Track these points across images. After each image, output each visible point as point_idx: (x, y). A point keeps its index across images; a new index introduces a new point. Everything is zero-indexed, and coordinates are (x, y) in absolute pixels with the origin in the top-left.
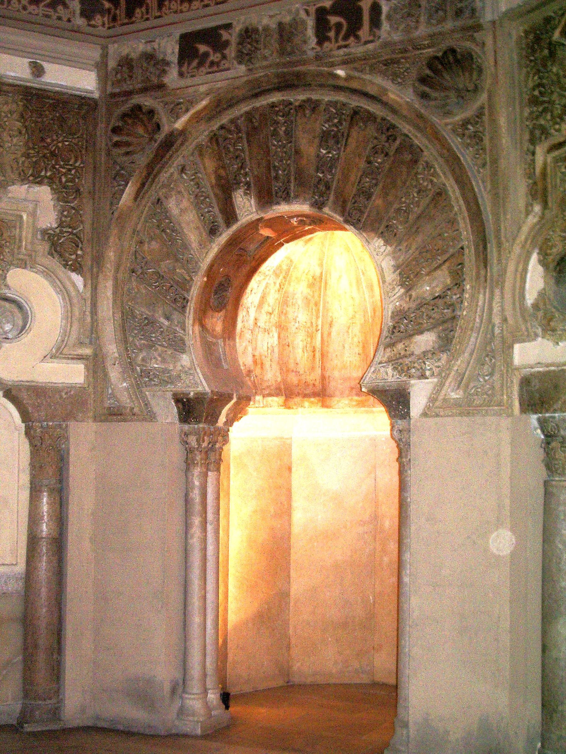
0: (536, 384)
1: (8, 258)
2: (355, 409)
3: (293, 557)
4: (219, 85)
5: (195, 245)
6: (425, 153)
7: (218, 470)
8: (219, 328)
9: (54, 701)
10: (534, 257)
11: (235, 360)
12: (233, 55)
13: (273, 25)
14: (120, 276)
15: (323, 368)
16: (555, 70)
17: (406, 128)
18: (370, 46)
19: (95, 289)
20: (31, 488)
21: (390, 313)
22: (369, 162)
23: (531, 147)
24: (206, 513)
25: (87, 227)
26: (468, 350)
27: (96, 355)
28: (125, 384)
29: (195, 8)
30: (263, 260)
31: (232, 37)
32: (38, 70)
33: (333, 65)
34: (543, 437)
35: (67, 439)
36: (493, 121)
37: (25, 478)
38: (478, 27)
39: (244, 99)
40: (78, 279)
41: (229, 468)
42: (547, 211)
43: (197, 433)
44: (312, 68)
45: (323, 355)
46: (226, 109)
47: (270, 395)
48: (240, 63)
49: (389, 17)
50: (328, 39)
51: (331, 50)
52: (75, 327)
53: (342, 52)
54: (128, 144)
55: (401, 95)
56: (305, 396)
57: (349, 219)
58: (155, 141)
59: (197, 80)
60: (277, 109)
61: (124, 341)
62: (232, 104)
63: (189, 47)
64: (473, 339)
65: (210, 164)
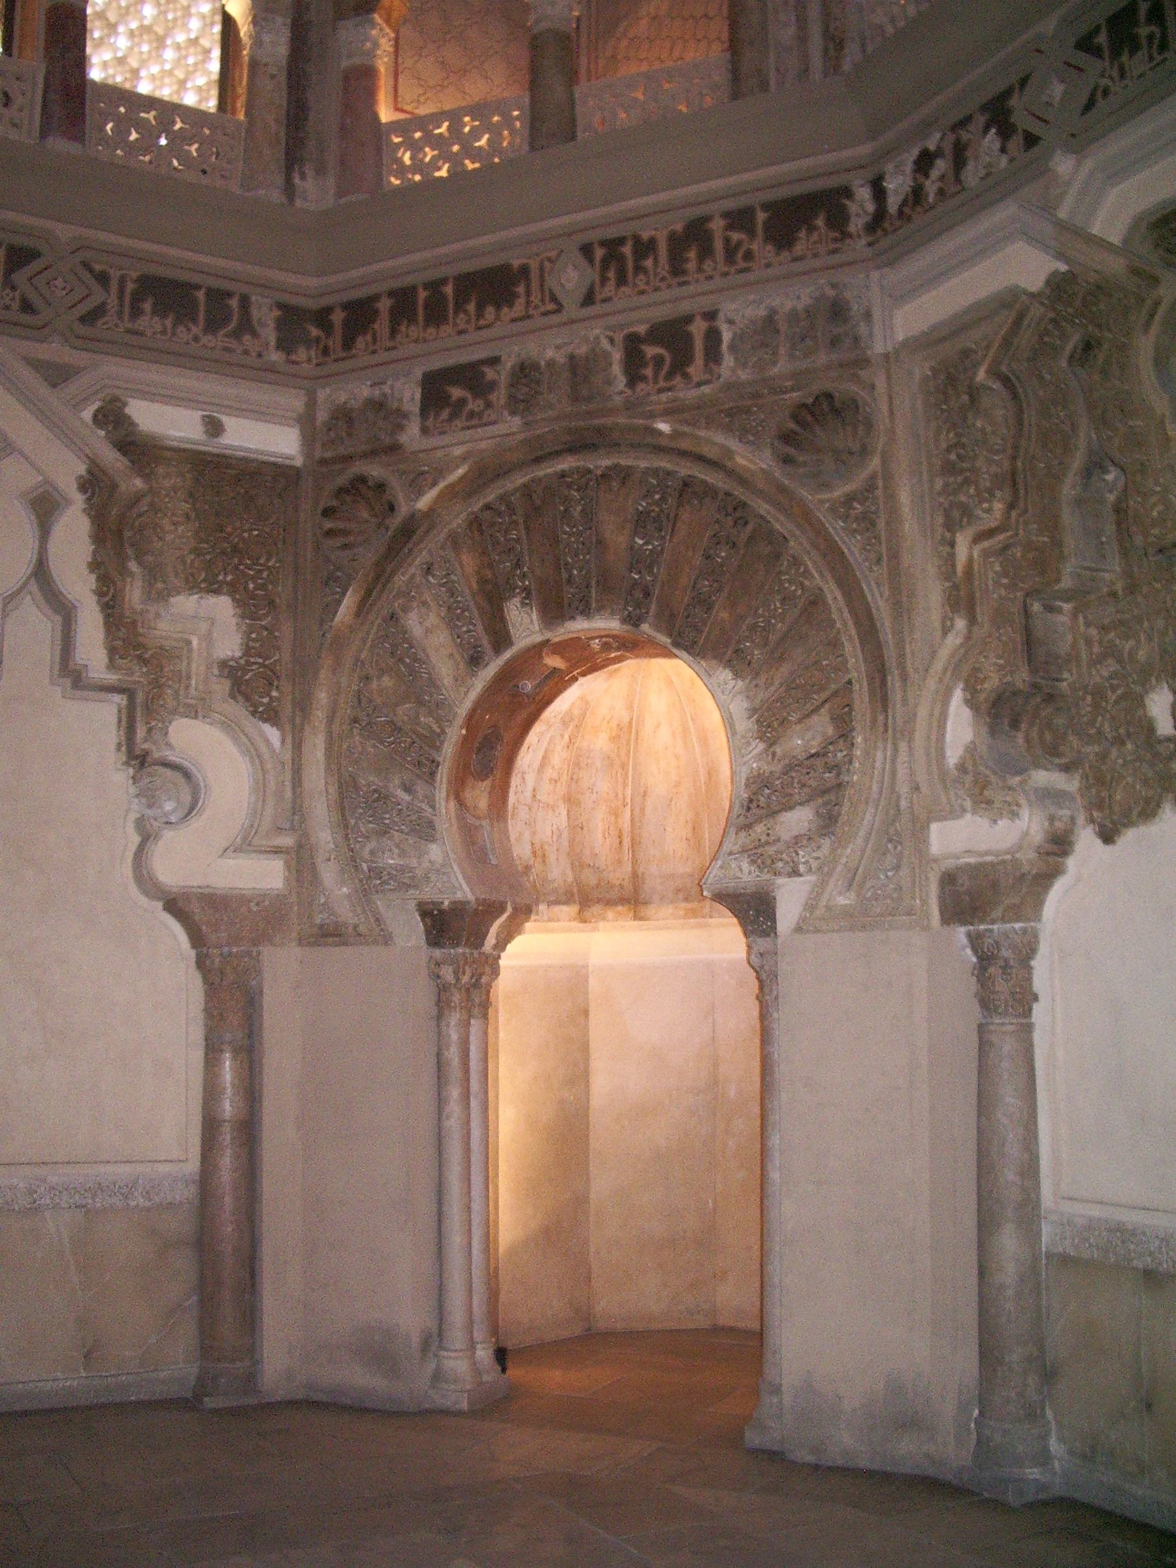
0: (964, 882)
1: (171, 703)
2: (681, 921)
3: (594, 1144)
4: (483, 445)
5: (447, 681)
6: (792, 543)
7: (485, 1016)
8: (483, 804)
9: (247, 1363)
10: (958, 695)
11: (508, 851)
12: (502, 402)
13: (561, 358)
14: (336, 727)
15: (635, 862)
16: (979, 424)
17: (763, 508)
18: (706, 389)
19: (298, 746)
20: (207, 1045)
21: (743, 781)
22: (708, 557)
23: (948, 535)
24: (468, 1080)
25: (284, 656)
26: (862, 833)
27: (300, 846)
28: (345, 890)
29: (444, 335)
30: (549, 702)
31: (501, 376)
32: (214, 427)
33: (652, 416)
34: (974, 959)
35: (259, 972)
36: (891, 497)
37: (197, 1033)
38: (863, 362)
39: (521, 466)
40: (273, 734)
41: (497, 1011)
42: (975, 629)
43: (453, 961)
44: (621, 420)
45: (635, 843)
46: (492, 481)
47: (557, 902)
48: (513, 413)
49: (732, 348)
50: (644, 379)
51: (649, 394)
52: (271, 802)
53: (664, 397)
54: (345, 533)
55: (753, 459)
56: (610, 903)
57: (679, 640)
58: (387, 529)
59: (446, 439)
60: (569, 480)
61: (344, 825)
62: (502, 472)
63: (435, 390)
64: (868, 817)
65: (469, 561)
